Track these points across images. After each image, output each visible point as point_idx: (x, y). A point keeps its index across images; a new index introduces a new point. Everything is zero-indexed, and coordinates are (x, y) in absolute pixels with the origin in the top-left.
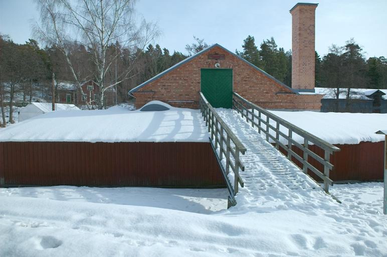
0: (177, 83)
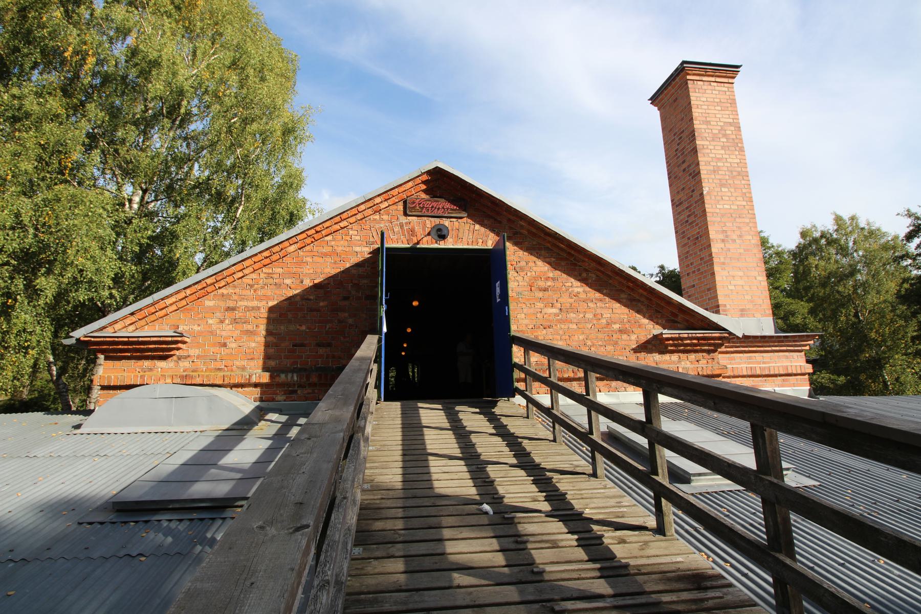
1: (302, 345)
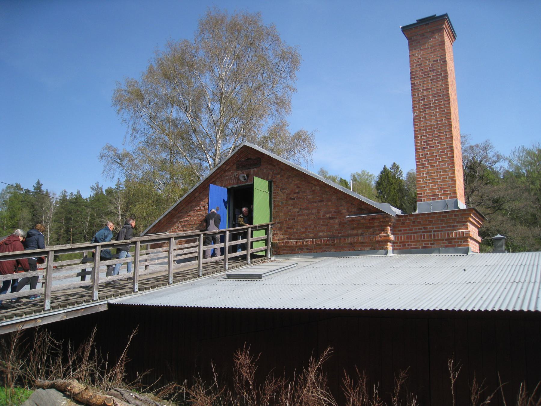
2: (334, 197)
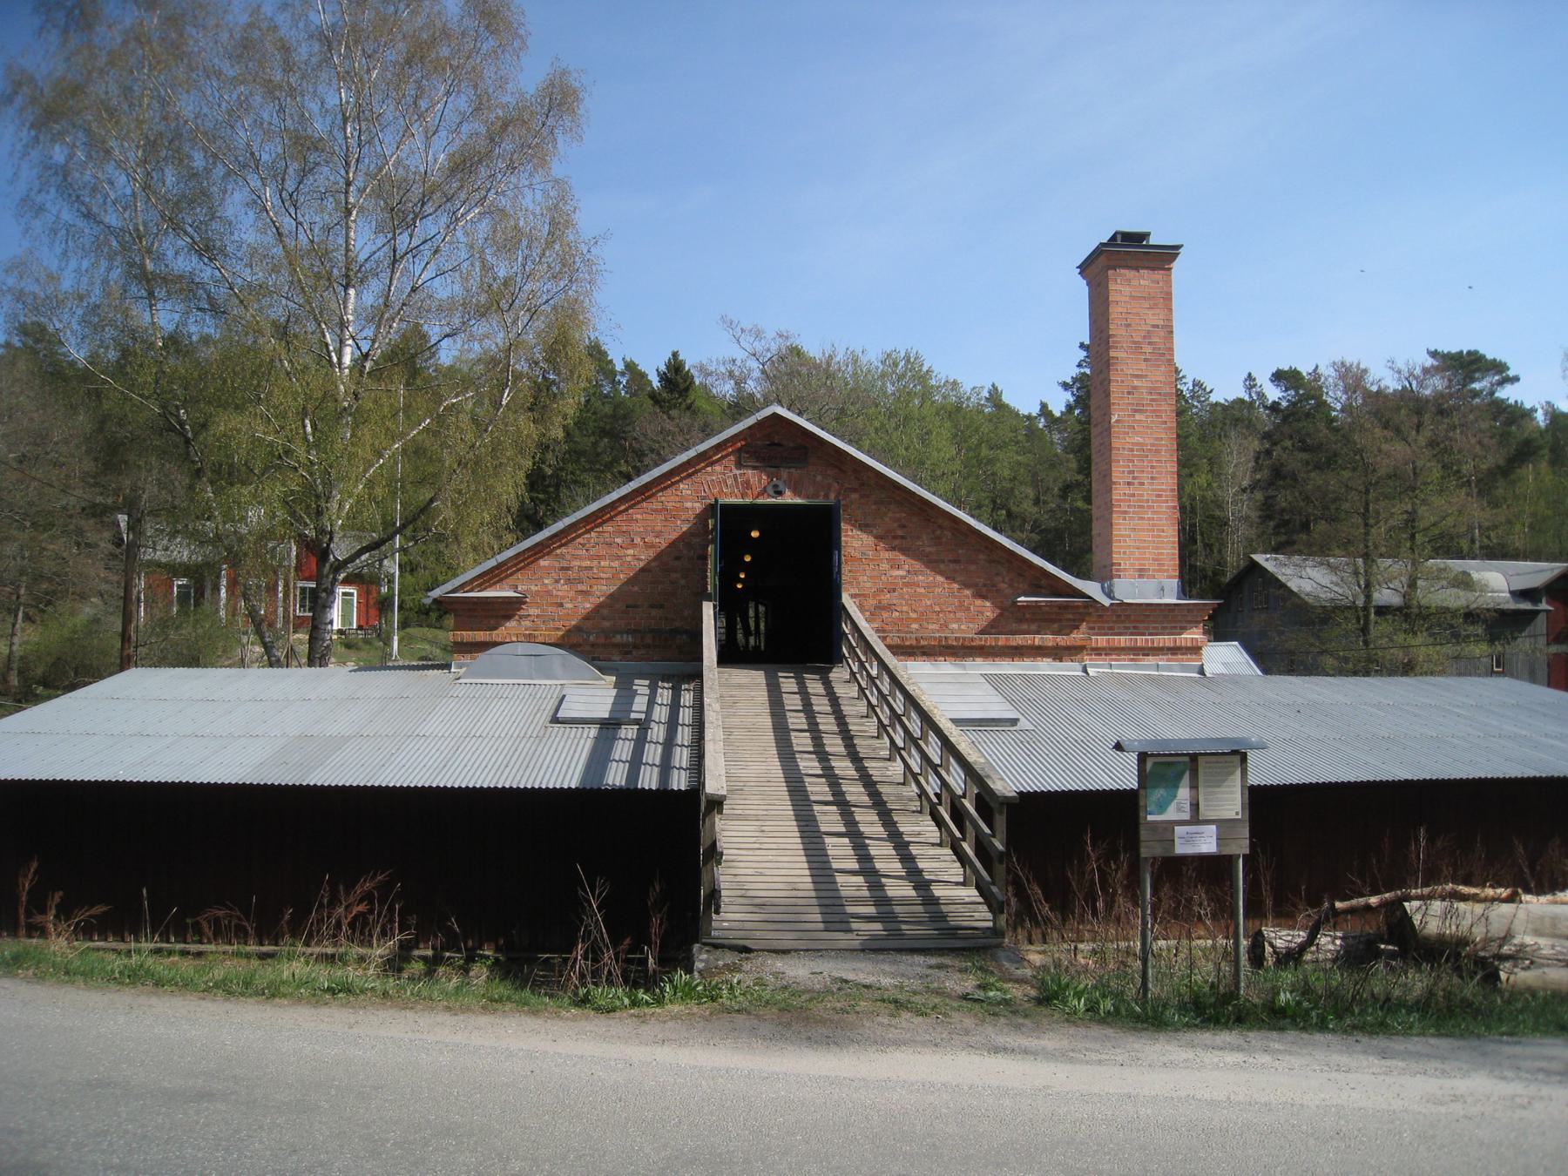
0: (619, 557)
1: (636, 606)
2: (981, 557)
